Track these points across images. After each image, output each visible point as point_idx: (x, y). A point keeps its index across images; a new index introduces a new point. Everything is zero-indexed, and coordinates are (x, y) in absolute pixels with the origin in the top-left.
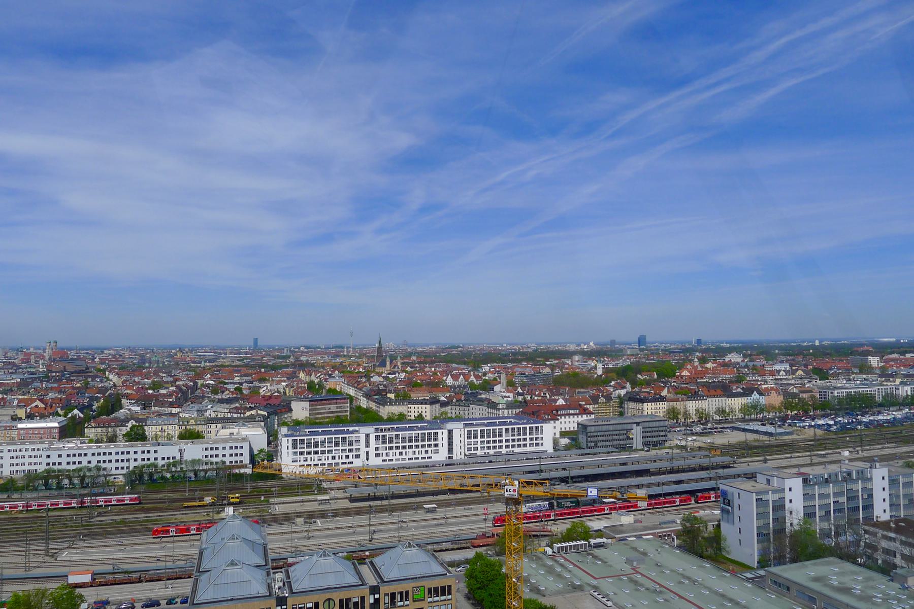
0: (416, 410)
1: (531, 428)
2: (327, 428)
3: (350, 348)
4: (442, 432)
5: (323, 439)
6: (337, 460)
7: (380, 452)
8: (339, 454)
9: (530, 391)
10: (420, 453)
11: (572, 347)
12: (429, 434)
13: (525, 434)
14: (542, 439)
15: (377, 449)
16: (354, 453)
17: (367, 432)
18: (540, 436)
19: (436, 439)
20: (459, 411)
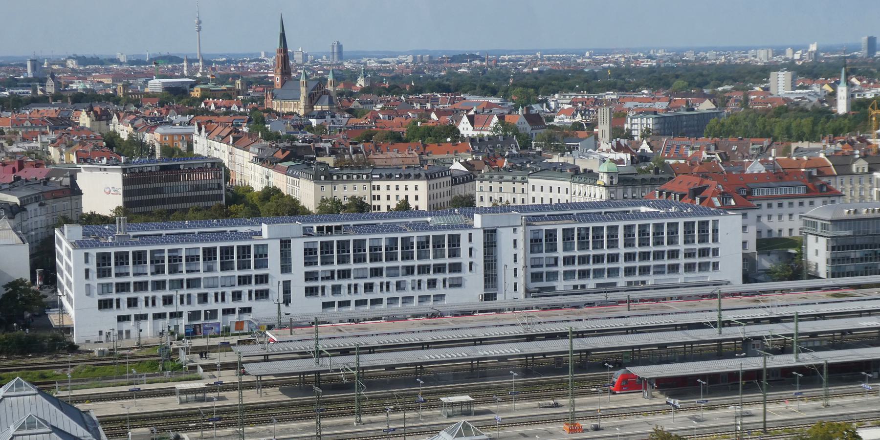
0: (393, 193)
1: (689, 226)
2: (180, 228)
3: (198, 61)
4: (470, 235)
5: (424, 240)
6: (211, 305)
7: (319, 284)
8: (216, 290)
9: (673, 150)
10: (385, 287)
11: (762, 58)
12: (598, 230)
13: (613, 243)
14: (715, 252)
15: (310, 277)
16: (254, 287)
17: (285, 236)
18: (711, 245)
19: (454, 253)
20: (501, 195)
